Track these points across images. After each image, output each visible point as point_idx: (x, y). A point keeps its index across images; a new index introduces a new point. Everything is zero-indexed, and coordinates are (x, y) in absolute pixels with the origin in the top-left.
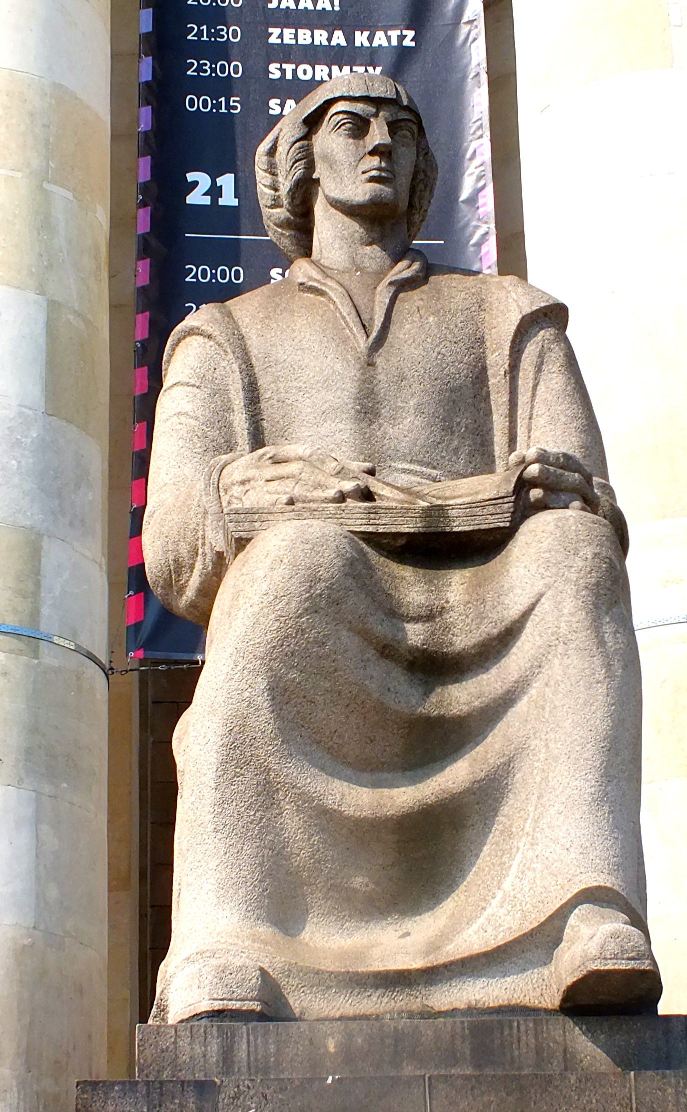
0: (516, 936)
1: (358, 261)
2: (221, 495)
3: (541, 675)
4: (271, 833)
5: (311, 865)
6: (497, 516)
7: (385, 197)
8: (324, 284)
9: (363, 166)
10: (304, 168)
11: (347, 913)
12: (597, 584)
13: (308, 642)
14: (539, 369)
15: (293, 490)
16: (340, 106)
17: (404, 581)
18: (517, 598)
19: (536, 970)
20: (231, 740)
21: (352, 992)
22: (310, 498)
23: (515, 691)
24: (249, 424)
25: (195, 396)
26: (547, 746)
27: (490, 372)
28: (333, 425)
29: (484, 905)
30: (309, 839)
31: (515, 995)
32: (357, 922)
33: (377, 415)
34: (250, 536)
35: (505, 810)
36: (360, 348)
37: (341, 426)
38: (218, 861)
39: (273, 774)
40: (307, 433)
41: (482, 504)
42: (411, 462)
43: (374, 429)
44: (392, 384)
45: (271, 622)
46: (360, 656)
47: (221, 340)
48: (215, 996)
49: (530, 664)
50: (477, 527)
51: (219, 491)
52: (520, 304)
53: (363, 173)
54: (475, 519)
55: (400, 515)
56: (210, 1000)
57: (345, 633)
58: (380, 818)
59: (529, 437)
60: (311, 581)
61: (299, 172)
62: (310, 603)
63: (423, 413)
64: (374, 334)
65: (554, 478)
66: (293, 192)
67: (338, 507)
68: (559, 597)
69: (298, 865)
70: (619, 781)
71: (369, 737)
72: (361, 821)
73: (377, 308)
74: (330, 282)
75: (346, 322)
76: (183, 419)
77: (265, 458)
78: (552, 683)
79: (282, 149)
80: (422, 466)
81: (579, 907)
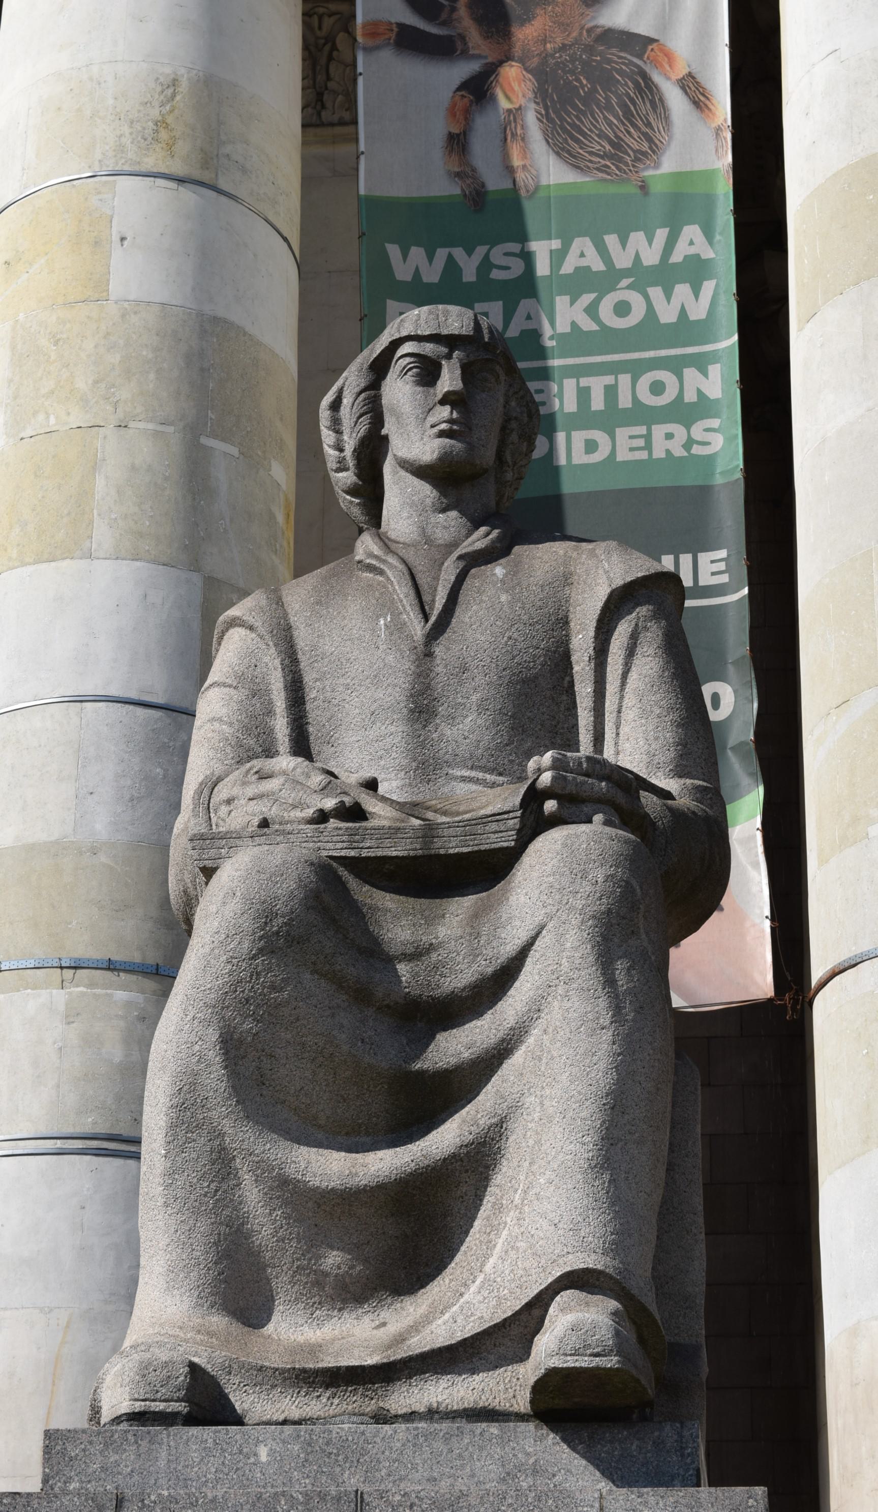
0: (485, 1327)
1: (429, 531)
2: (212, 817)
3: (540, 1021)
4: (228, 1207)
5: (274, 1244)
6: (501, 835)
7: (457, 454)
8: (384, 561)
9: (431, 420)
10: (370, 423)
11: (316, 1299)
12: (609, 911)
13: (265, 987)
14: (631, 653)
15: (270, 810)
16: (407, 348)
17: (389, 914)
18: (515, 931)
19: (510, 1367)
20: (182, 1100)
21: (299, 1392)
22: (287, 818)
23: (511, 1040)
24: (291, 729)
25: (231, 699)
26: (542, 1104)
27: (574, 658)
28: (383, 728)
29: (463, 1290)
30: (270, 1214)
31: (483, 1397)
32: (329, 1310)
33: (434, 714)
34: (215, 866)
35: (498, 1180)
36: (416, 635)
37: (392, 729)
38: (168, 1240)
39: (228, 1139)
40: (354, 739)
41: (484, 820)
42: (472, 768)
43: (429, 731)
44: (451, 677)
45: (222, 965)
46: (327, 1002)
47: (262, 630)
48: (136, 1396)
49: (527, 1008)
50: (476, 848)
51: (209, 812)
52: (612, 575)
53: (432, 426)
54: (475, 839)
55: (387, 836)
56: (130, 1400)
57: (308, 976)
58: (351, 1189)
59: (618, 734)
60: (267, 917)
61: (363, 428)
62: (265, 943)
63: (487, 709)
64: (433, 619)
65: (573, 787)
66: (359, 453)
67: (316, 829)
68: (561, 929)
69: (260, 1244)
70: (626, 1144)
71: (342, 1096)
72: (329, 1192)
73: (440, 588)
74: (391, 559)
75: (403, 606)
76: (217, 725)
77: (252, 772)
78: (550, 1030)
79: (346, 401)
80: (485, 772)
81: (562, 1293)
